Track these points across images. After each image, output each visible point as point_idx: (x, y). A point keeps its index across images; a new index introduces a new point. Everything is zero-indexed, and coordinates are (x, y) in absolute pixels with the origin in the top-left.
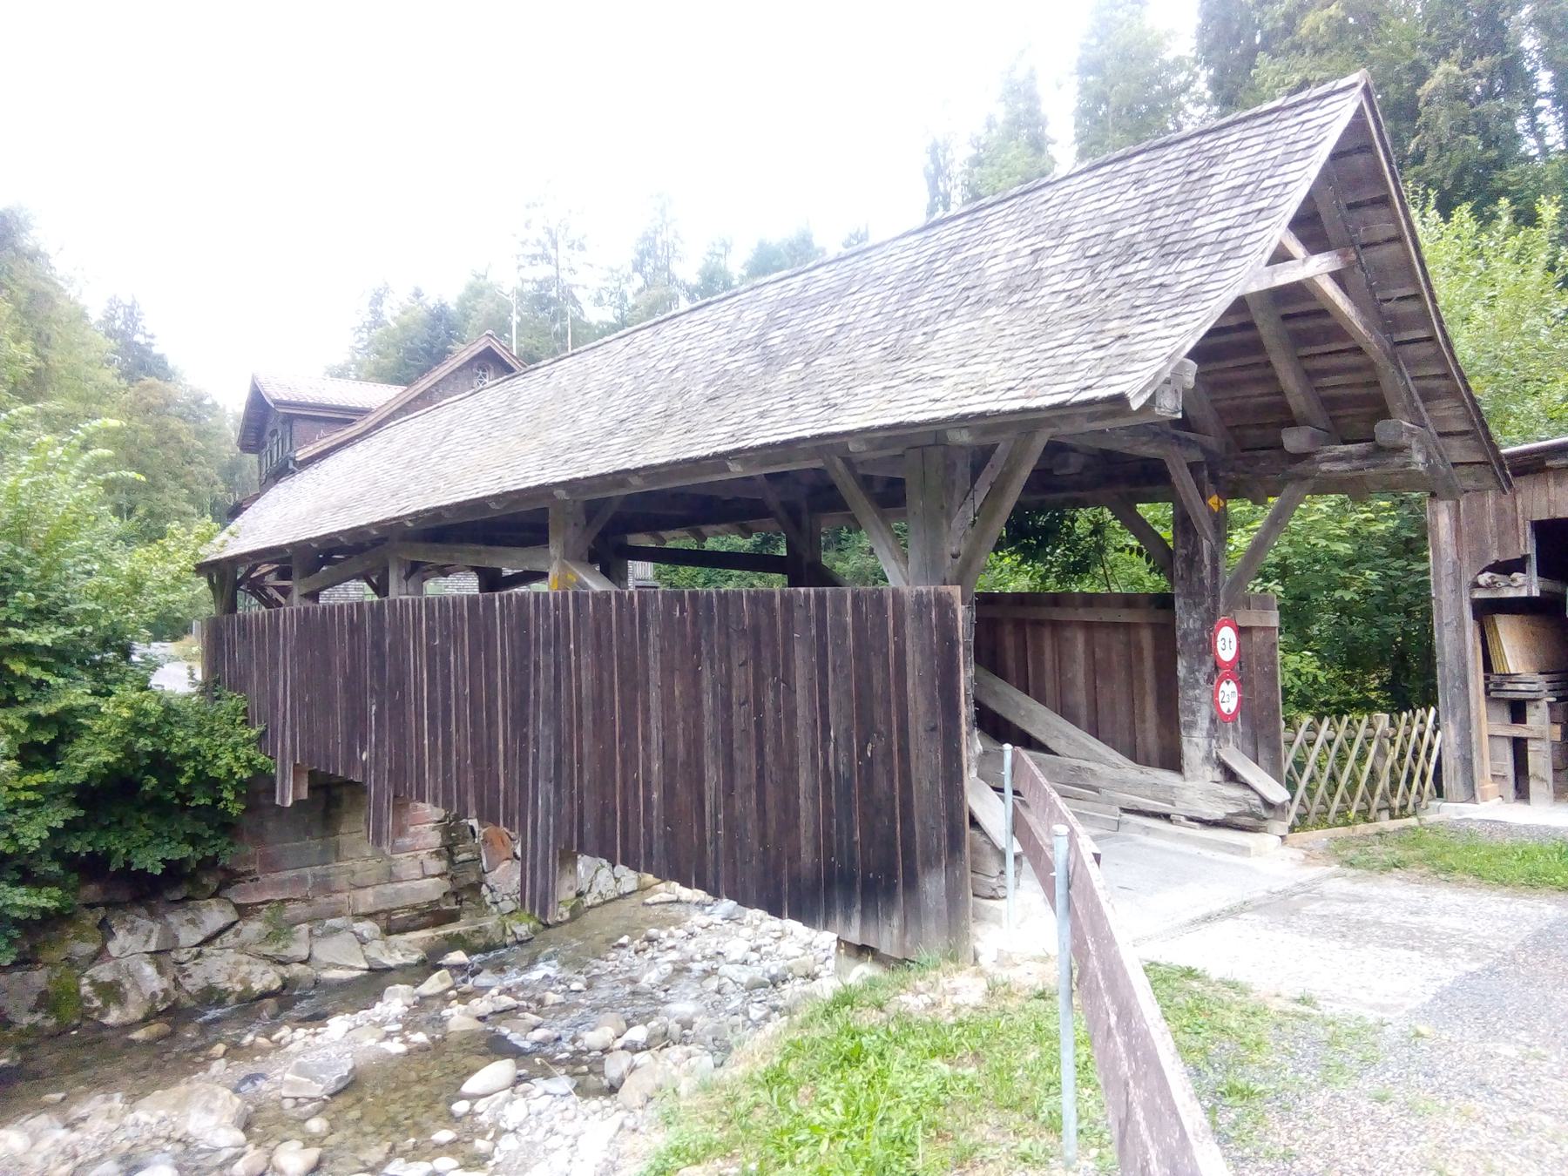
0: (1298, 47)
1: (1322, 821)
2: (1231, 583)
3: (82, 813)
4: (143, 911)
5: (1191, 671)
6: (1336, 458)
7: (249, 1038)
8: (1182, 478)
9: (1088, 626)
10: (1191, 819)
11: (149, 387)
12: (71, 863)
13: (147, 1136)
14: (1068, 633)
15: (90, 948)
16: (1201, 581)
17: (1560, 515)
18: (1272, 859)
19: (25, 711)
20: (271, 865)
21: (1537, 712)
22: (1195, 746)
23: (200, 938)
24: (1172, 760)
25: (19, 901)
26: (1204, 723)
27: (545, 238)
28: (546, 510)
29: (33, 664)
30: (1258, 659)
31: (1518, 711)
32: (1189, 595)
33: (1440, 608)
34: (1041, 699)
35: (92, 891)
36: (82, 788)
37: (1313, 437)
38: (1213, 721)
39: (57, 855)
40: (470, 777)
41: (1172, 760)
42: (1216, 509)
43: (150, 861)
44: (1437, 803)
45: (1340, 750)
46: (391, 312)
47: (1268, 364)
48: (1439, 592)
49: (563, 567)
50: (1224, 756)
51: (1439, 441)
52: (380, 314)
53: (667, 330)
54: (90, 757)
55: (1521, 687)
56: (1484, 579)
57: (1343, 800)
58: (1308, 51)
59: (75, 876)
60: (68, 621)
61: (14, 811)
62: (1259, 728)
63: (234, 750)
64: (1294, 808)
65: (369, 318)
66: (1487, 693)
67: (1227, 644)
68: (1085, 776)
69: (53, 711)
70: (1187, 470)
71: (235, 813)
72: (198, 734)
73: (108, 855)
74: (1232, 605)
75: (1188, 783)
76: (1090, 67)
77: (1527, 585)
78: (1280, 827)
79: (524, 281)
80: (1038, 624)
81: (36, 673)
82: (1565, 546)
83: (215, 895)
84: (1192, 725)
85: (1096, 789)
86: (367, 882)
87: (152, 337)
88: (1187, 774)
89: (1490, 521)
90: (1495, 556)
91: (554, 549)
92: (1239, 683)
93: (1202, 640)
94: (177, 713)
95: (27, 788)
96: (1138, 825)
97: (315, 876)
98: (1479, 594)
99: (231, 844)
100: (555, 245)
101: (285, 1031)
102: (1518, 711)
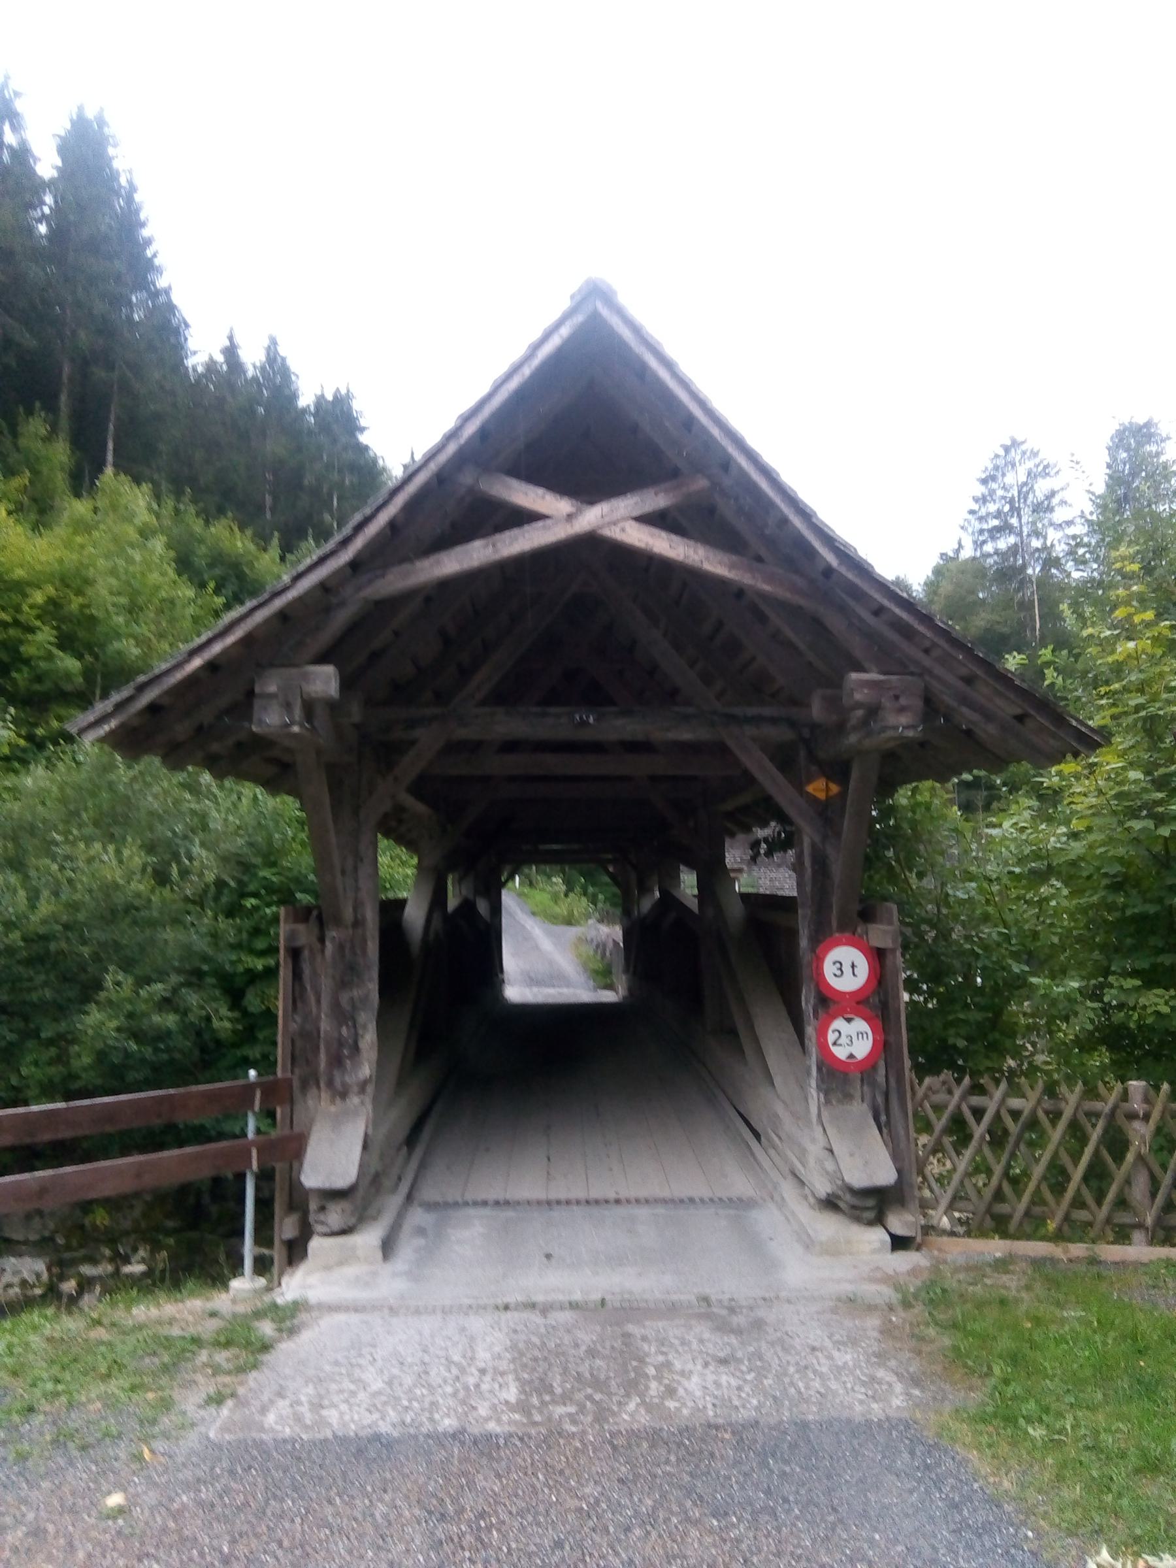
42: (822, 796)
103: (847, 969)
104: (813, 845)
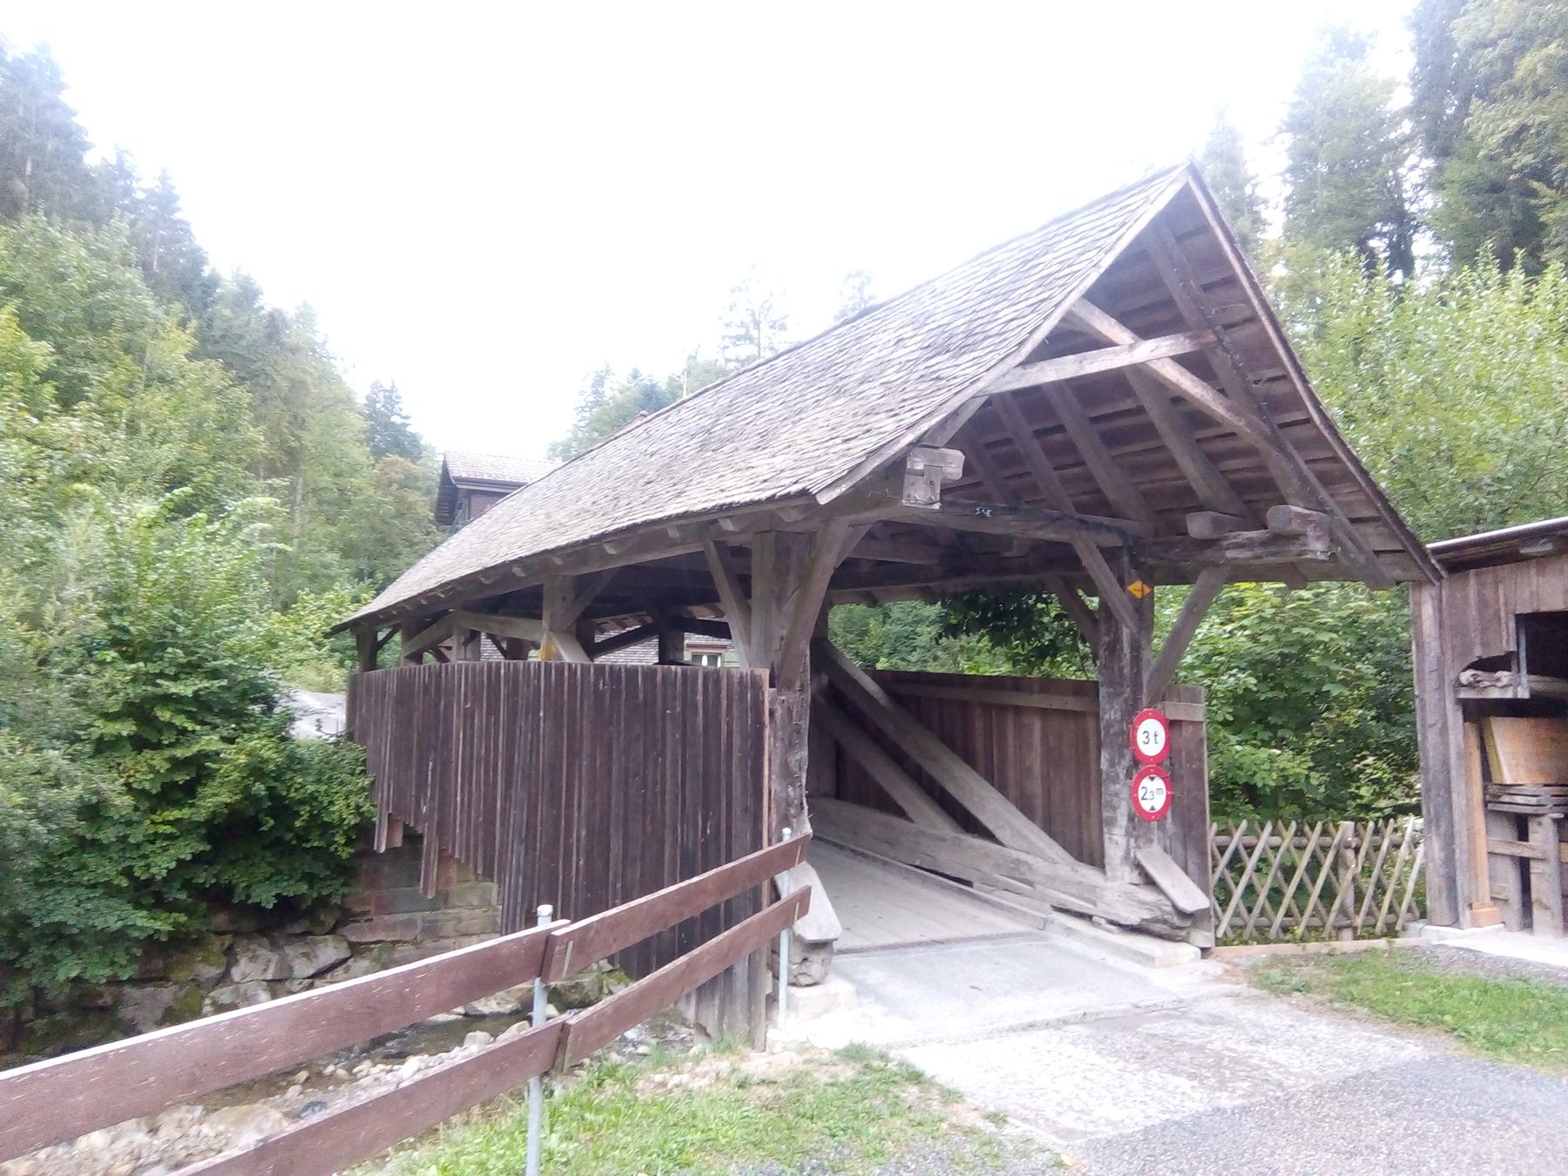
0: (1516, 91)
1: (1262, 936)
2: (1157, 670)
3: (208, 847)
4: (265, 941)
5: (1112, 764)
6: (1241, 544)
7: (331, 1068)
8: (1095, 565)
9: (1044, 713)
10: (1112, 922)
11: (393, 463)
12: (200, 892)
13: (203, 1147)
14: (1027, 719)
15: (215, 972)
16: (1121, 669)
17: (1543, 609)
18: (1179, 970)
19: (168, 753)
20: (385, 908)
21: (1540, 829)
22: (1116, 843)
23: (312, 972)
24: (1093, 857)
25: (139, 923)
26: (1123, 821)
27: (748, 320)
28: (541, 586)
29: (178, 712)
30: (1188, 754)
31: (1521, 825)
32: (1111, 684)
33: (1423, 708)
34: (1003, 789)
35: (221, 920)
36: (207, 823)
37: (1217, 524)
38: (1131, 819)
39: (187, 885)
40: (481, 834)
41: (1093, 857)
42: (1139, 595)
43: (266, 896)
44: (1419, 925)
45: (1314, 856)
46: (611, 390)
47: (1163, 448)
48: (1423, 691)
49: (549, 639)
50: (1139, 856)
51: (1351, 528)
52: (601, 395)
53: (673, 417)
54: (215, 798)
55: (1519, 799)
56: (1466, 677)
57: (1288, 914)
58: (1528, 93)
59: (204, 906)
60: (215, 674)
61: (153, 843)
62: (1184, 829)
63: (347, 798)
64: (1226, 919)
65: (591, 398)
66: (1486, 803)
67: (1151, 737)
68: (1023, 869)
69: (189, 754)
70: (1099, 555)
71: (344, 856)
72: (319, 781)
73: (230, 889)
74: (1160, 697)
75: (1109, 884)
76: (1298, 125)
77: (1516, 685)
78: (1203, 937)
79: (728, 360)
80: (1003, 708)
81: (180, 721)
82: (1558, 641)
83: (332, 931)
84: (1112, 822)
85: (1030, 884)
86: (472, 930)
87: (407, 418)
88: (1109, 874)
89: (1473, 612)
90: (1478, 652)
91: (545, 623)
92: (1170, 782)
93: (1121, 733)
94: (301, 761)
95: (165, 823)
96: (1061, 925)
97: (423, 920)
98: (1465, 694)
99: (345, 884)
100: (757, 324)
101: (365, 1066)
102: (1521, 825)
103: (1152, 738)
104: (1132, 635)
